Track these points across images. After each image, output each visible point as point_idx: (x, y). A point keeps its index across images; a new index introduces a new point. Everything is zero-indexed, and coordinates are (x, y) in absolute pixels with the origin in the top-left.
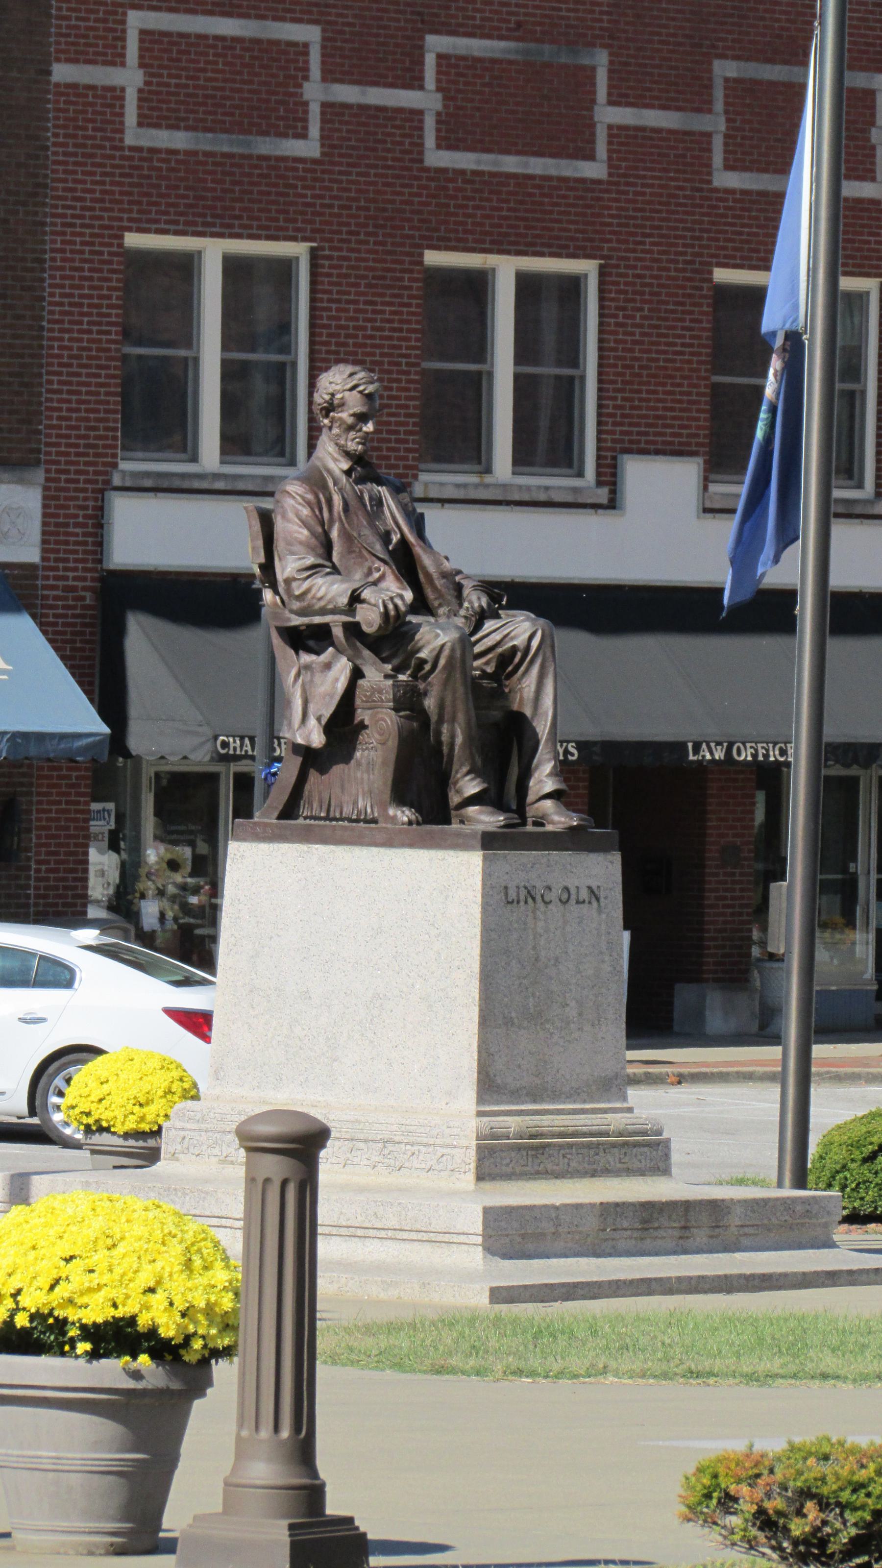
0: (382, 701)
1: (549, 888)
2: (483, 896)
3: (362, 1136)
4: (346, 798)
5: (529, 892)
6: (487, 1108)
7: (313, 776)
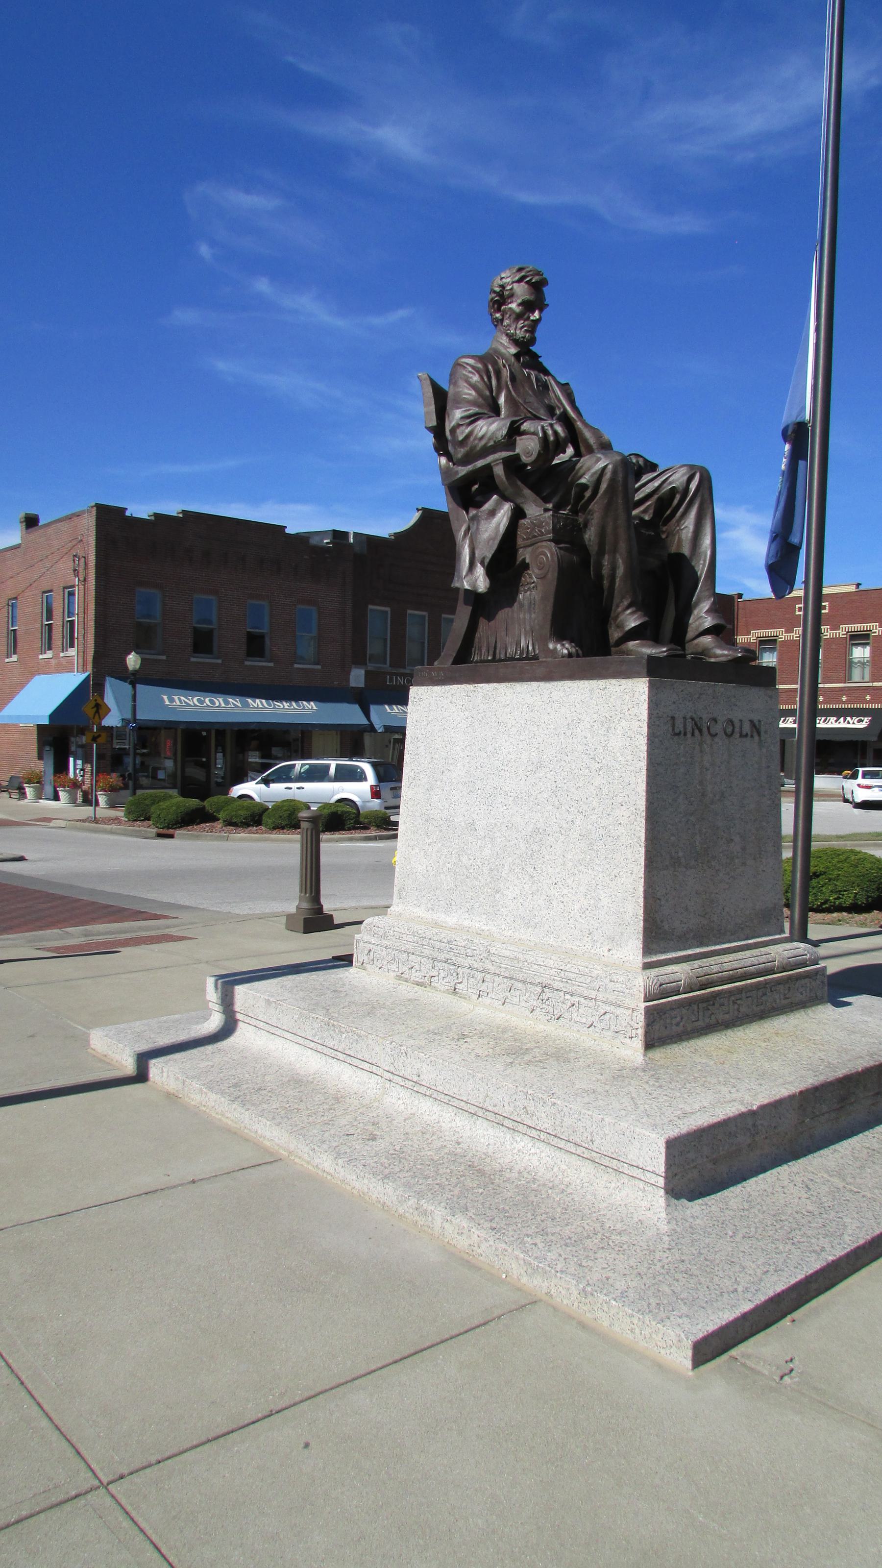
0: (542, 534)
1: (715, 720)
2: (650, 725)
3: (520, 976)
4: (509, 640)
5: (696, 724)
6: (654, 958)
7: (483, 623)
